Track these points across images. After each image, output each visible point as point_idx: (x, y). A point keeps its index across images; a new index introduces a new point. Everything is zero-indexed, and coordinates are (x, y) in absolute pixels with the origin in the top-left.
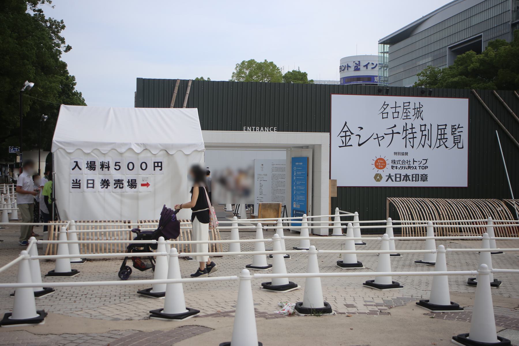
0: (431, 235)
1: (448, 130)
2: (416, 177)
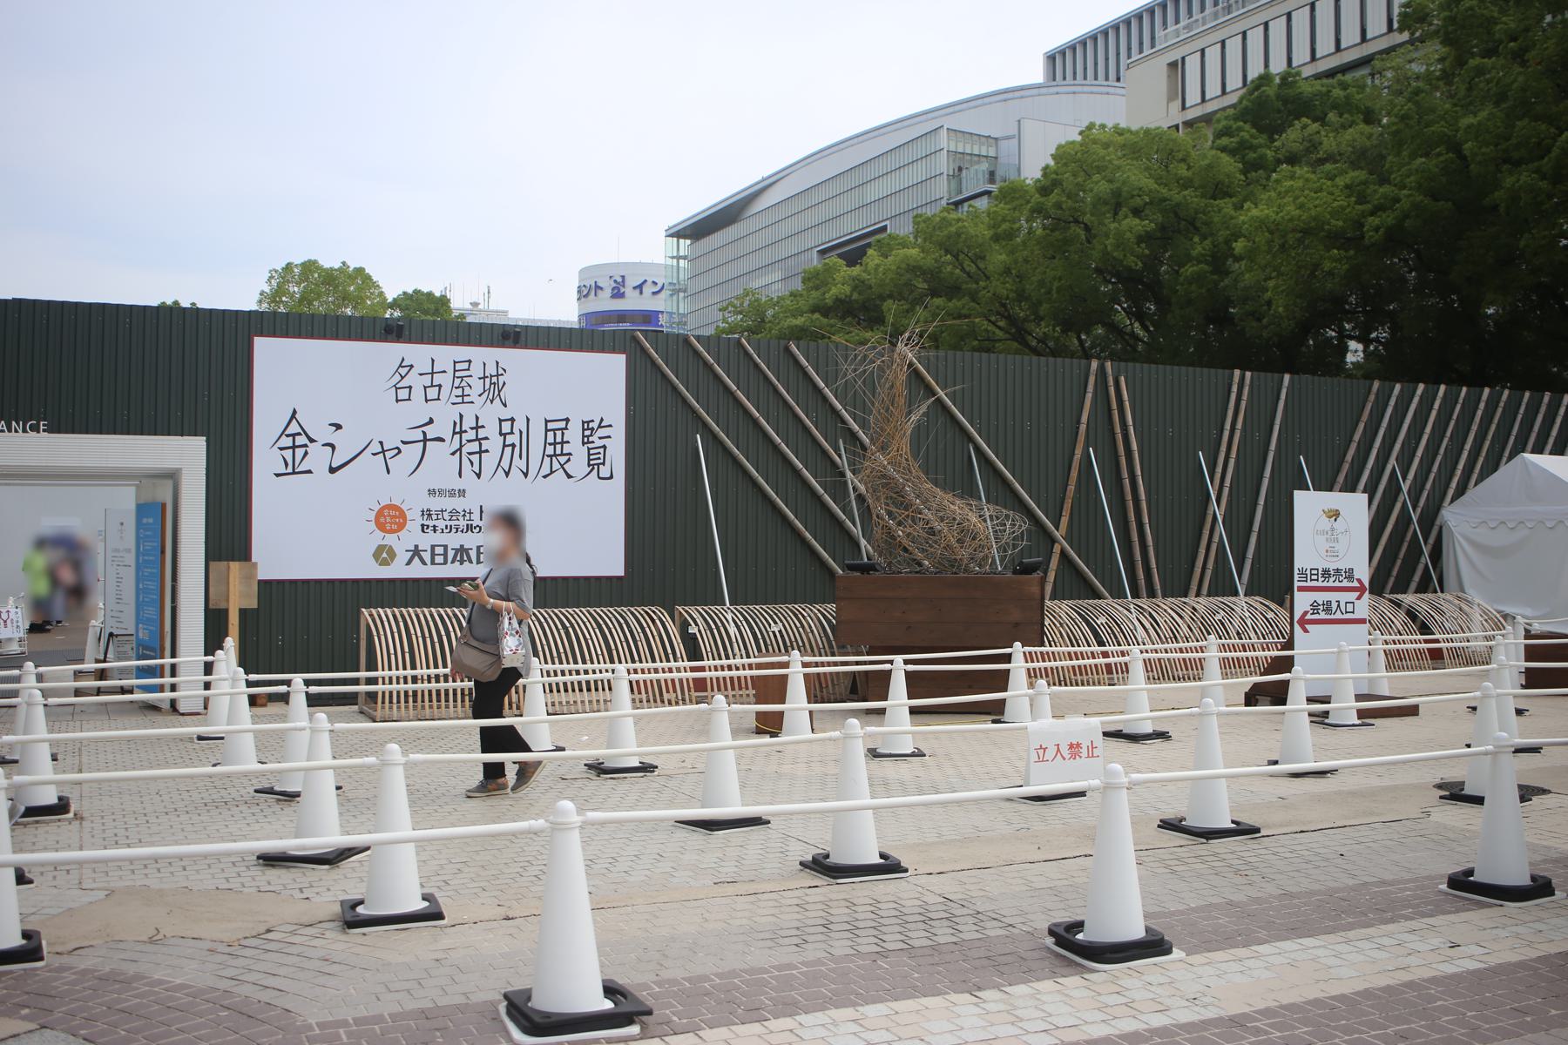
1: (574, 434)
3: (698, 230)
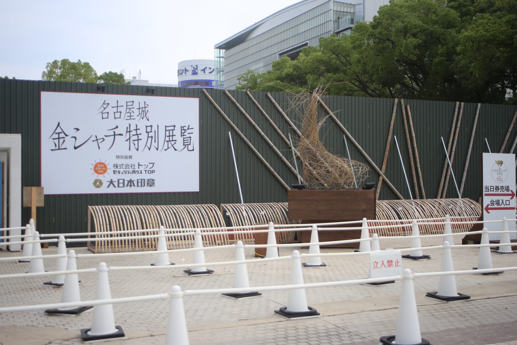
0: (315, 241)
1: (177, 132)
2: (142, 183)
3: (228, 45)
